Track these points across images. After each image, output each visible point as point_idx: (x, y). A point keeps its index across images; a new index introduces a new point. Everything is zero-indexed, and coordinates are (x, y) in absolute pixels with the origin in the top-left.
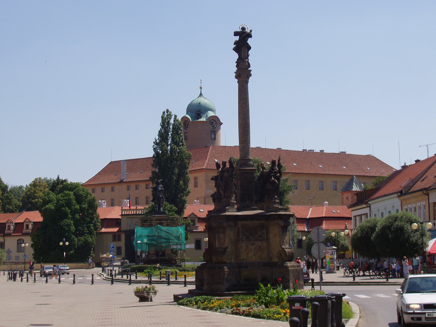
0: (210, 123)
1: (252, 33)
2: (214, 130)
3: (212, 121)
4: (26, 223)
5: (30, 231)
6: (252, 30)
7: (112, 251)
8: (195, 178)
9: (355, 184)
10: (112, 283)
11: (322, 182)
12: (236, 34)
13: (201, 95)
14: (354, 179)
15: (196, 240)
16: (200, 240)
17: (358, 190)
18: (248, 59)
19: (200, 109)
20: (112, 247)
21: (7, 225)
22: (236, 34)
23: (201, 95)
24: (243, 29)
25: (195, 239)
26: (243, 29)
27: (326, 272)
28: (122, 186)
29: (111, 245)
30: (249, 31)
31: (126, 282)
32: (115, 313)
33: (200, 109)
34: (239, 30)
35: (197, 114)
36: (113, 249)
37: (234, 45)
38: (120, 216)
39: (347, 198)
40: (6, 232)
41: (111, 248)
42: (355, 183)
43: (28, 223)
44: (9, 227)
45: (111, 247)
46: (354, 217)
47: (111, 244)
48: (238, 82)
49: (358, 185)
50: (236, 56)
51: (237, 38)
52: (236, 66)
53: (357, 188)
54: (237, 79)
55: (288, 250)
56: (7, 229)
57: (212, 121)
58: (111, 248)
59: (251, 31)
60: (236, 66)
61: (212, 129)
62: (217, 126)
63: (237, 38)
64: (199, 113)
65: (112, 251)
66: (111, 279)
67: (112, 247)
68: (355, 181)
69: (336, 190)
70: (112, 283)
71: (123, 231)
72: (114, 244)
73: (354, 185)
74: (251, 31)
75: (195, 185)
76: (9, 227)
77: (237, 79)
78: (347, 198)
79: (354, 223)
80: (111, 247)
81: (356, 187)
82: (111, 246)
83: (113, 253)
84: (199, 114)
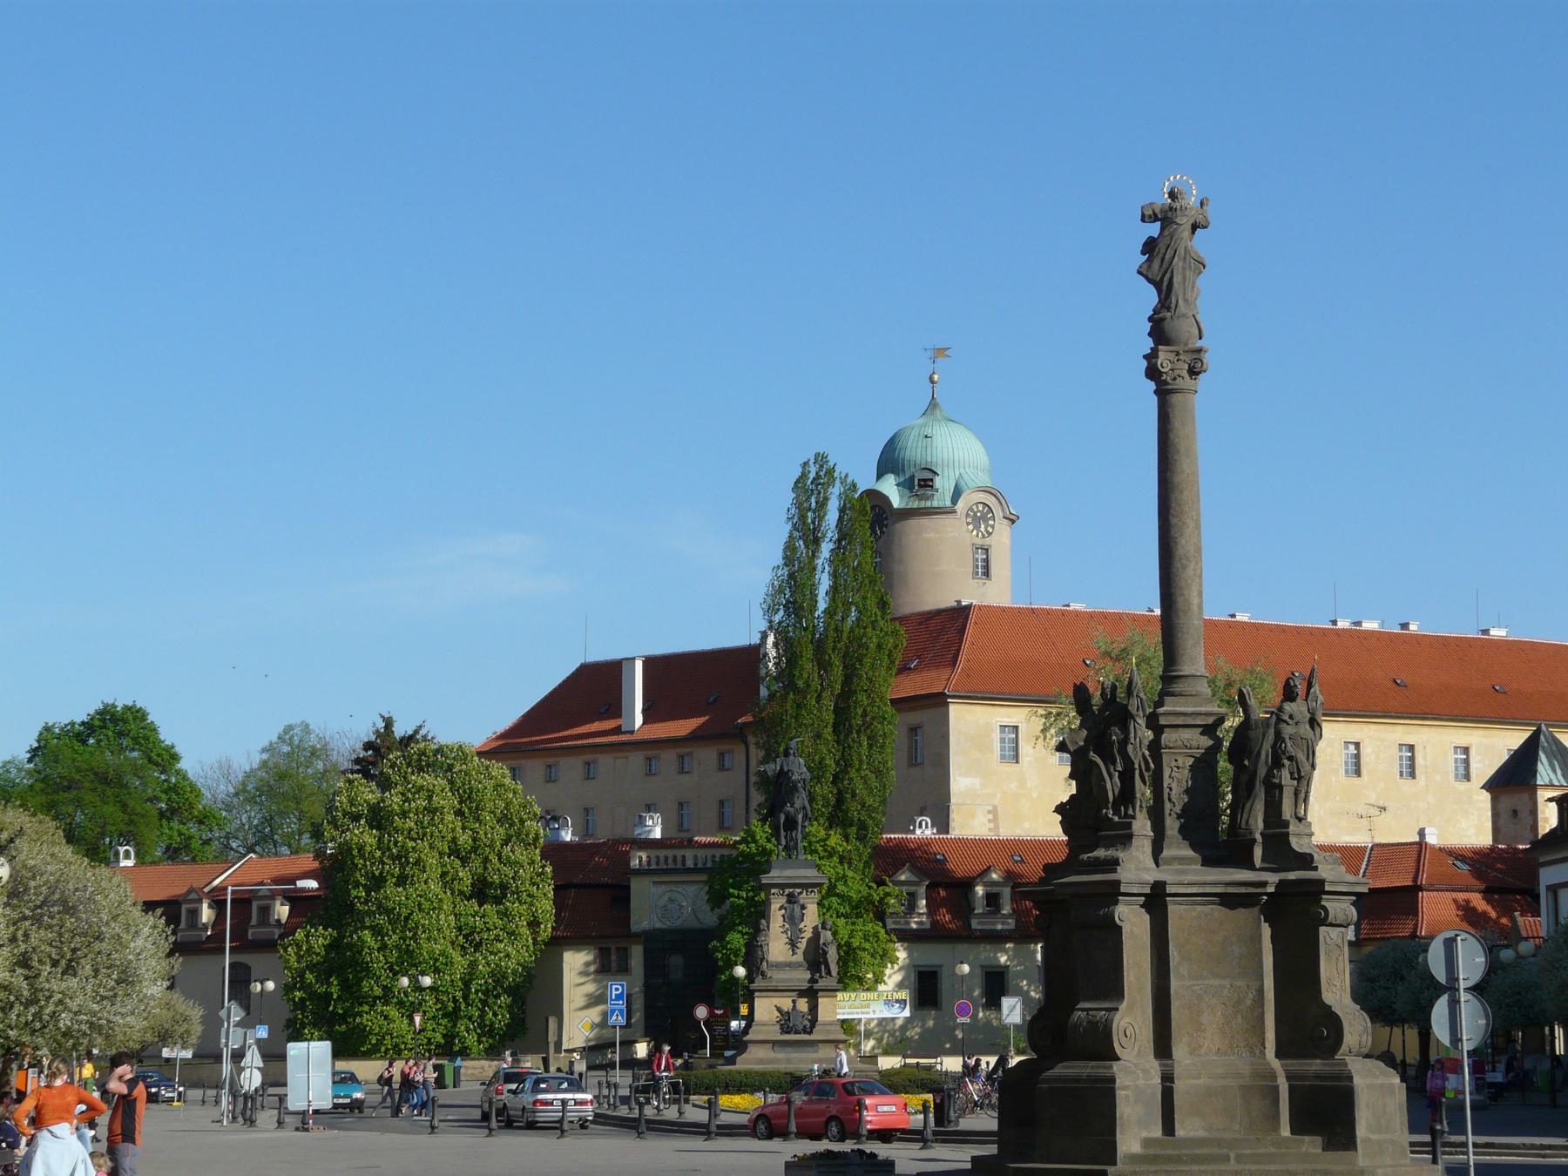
0: (967, 515)
2: (987, 541)
3: (977, 507)
4: (188, 903)
5: (274, 933)
7: (615, 1010)
8: (911, 729)
9: (1547, 757)
11: (1411, 748)
14: (1542, 737)
15: (921, 969)
16: (934, 969)
17: (1559, 782)
19: (929, 459)
20: (616, 995)
21: (184, 907)
23: (933, 404)
25: (982, 967)
28: (627, 758)
29: (614, 987)
36: (621, 1002)
37: (1142, 256)
39: (1515, 812)
40: (182, 935)
41: (611, 1000)
42: (1545, 753)
43: (268, 902)
44: (192, 919)
45: (614, 997)
46: (1549, 888)
47: (611, 985)
48: (1155, 392)
49: (1556, 763)
52: (1150, 334)
53: (1554, 771)
54: (1153, 383)
56: (254, 921)
57: (977, 507)
58: (611, 1000)
60: (1150, 334)
61: (979, 541)
65: (615, 1010)
67: (616, 995)
68: (1546, 744)
69: (1467, 777)
71: (637, 935)
72: (622, 985)
73: (1542, 764)
75: (910, 759)
76: (192, 919)
77: (1152, 380)
78: (1515, 812)
79: (1548, 913)
80: (614, 997)
81: (1548, 767)
82: (614, 993)
83: (620, 1018)
84: (925, 480)
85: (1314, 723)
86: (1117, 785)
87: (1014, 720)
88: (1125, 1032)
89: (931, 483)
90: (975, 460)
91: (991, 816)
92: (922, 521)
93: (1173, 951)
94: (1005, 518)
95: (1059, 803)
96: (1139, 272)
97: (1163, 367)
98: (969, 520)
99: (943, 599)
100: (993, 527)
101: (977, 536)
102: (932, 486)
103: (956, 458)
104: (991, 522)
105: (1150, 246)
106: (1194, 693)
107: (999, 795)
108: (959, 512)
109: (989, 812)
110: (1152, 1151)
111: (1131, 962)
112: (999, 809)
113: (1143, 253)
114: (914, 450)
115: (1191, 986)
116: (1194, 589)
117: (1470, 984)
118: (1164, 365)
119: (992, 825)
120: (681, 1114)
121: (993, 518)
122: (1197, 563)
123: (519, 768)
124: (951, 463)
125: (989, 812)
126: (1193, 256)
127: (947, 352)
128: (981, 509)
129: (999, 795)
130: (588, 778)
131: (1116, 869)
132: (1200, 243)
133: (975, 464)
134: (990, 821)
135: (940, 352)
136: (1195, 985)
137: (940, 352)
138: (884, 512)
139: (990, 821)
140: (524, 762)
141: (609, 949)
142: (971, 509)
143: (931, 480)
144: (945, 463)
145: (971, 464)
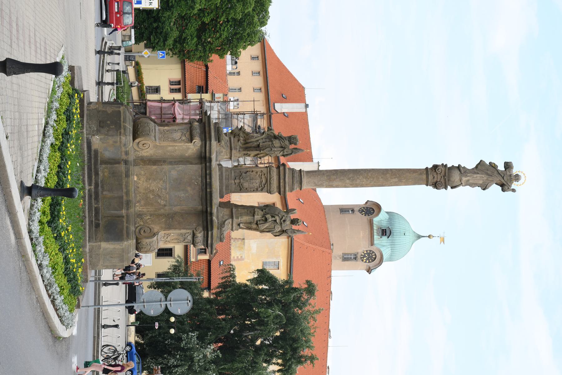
0: (370, 251)
1: (509, 194)
3: (374, 255)
6: (515, 192)
10: (98, 52)
12: (508, 166)
13: (419, 237)
18: (465, 185)
19: (395, 234)
22: (508, 166)
23: (419, 237)
24: (517, 178)
26: (517, 178)
27: (148, 12)
30: (513, 187)
31: (98, 95)
32: (38, 113)
33: (395, 234)
34: (515, 171)
35: (386, 230)
38: (213, 91)
50: (470, 165)
51: (501, 168)
55: (154, 242)
57: (374, 255)
59: (514, 190)
62: (366, 264)
63: (501, 168)
64: (388, 234)
66: (104, 49)
70: (98, 52)
74: (514, 190)
85: (283, 232)
86: (253, 144)
87: (282, 268)
88: (146, 144)
89: (384, 234)
90: (394, 254)
91: (239, 258)
92: (367, 231)
93: (181, 167)
94: (370, 267)
95: (246, 49)
96: (481, 161)
97: (438, 170)
98: (368, 252)
99: (334, 237)
100: (366, 262)
101: (361, 255)
102: (383, 235)
103: (396, 246)
104: (367, 261)
105: (493, 166)
106: (294, 183)
107: (249, 261)
108: (371, 247)
109: (241, 257)
110: (93, 153)
111: (176, 148)
112: (243, 261)
113: (490, 163)
114: (399, 241)
115: (166, 176)
116: (340, 183)
117: (169, 306)
118: (439, 170)
119: (236, 258)
120: (109, 63)
121: (369, 262)
122: (351, 185)
123: (258, 60)
124: (394, 244)
125: (241, 257)
126: (489, 184)
127: (442, 242)
128: (373, 257)
129: (249, 261)
130: (254, 90)
131: (217, 141)
132: (495, 189)
133: (393, 254)
134: (238, 257)
135: (443, 240)
136: (167, 177)
137: (443, 240)
138: (371, 215)
139: (238, 257)
140: (261, 61)
141: (180, 85)
142: (373, 252)
143: (386, 235)
144: (393, 241)
145: (393, 253)
